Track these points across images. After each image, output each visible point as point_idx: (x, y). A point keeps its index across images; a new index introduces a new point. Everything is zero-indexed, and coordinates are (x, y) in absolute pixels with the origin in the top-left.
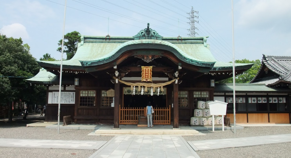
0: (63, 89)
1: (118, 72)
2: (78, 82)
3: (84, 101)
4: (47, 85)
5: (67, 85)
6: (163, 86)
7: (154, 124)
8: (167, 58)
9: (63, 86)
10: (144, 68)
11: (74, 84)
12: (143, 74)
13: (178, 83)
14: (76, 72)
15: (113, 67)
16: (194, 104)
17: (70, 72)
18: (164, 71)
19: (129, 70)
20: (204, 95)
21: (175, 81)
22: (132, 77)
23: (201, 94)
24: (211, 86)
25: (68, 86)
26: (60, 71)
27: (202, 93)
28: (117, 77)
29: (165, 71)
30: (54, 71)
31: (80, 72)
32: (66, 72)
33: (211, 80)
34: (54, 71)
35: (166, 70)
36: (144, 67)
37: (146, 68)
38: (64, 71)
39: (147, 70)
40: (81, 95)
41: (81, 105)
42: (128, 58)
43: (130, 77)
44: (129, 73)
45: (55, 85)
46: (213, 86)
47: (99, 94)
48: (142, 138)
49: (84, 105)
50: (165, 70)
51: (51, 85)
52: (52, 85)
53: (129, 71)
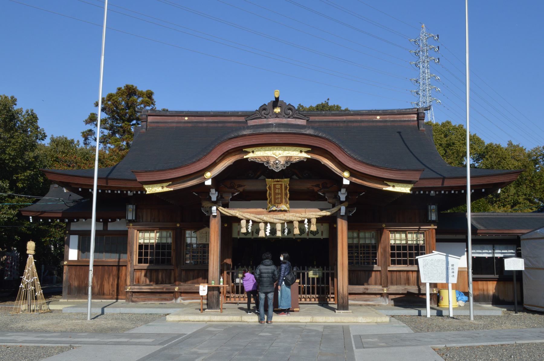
0: (101, 228)
1: (216, 191)
2: (134, 212)
3: (163, 254)
4: (67, 220)
5: (110, 220)
6: (317, 219)
7: (275, 309)
8: (318, 162)
9: (101, 220)
10: (273, 183)
11: (125, 217)
12: (270, 194)
13: (346, 213)
14: (129, 192)
15: (204, 182)
16: (391, 259)
17: (116, 192)
18: (316, 189)
19: (240, 186)
20: (365, 238)
21: (340, 210)
22: (251, 201)
23: (358, 237)
24: (430, 219)
25: (114, 220)
26: (93, 190)
27: (362, 234)
28: (215, 203)
29: (318, 189)
30: (80, 190)
31: (137, 192)
32: (106, 191)
33: (429, 206)
34: (80, 190)
35: (321, 186)
36: (271, 181)
37: (276, 183)
38: (103, 191)
39: (278, 186)
40: (392, 242)
41: (393, 262)
42: (236, 163)
43: (246, 200)
44: (241, 194)
45: (84, 220)
46: (433, 219)
47: (179, 237)
48: (273, 347)
49: (399, 263)
50: (318, 186)
51: (75, 220)
52: (78, 220)
53: (241, 189)
